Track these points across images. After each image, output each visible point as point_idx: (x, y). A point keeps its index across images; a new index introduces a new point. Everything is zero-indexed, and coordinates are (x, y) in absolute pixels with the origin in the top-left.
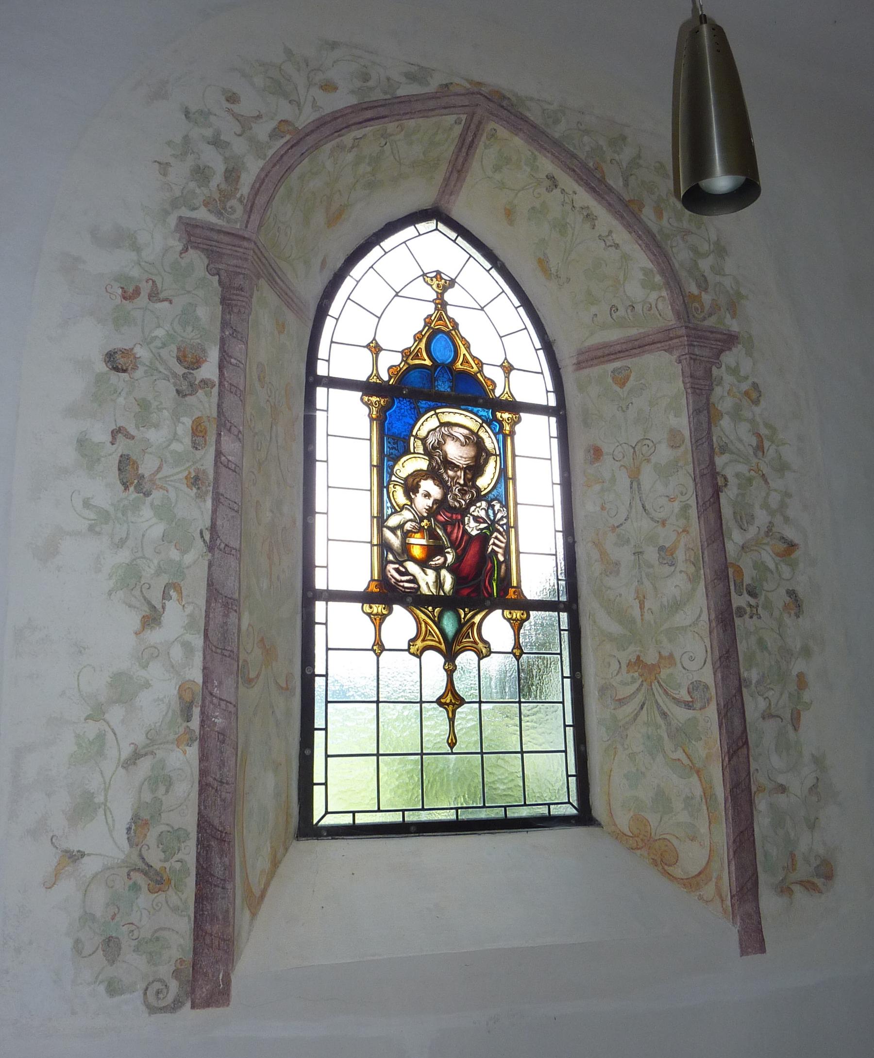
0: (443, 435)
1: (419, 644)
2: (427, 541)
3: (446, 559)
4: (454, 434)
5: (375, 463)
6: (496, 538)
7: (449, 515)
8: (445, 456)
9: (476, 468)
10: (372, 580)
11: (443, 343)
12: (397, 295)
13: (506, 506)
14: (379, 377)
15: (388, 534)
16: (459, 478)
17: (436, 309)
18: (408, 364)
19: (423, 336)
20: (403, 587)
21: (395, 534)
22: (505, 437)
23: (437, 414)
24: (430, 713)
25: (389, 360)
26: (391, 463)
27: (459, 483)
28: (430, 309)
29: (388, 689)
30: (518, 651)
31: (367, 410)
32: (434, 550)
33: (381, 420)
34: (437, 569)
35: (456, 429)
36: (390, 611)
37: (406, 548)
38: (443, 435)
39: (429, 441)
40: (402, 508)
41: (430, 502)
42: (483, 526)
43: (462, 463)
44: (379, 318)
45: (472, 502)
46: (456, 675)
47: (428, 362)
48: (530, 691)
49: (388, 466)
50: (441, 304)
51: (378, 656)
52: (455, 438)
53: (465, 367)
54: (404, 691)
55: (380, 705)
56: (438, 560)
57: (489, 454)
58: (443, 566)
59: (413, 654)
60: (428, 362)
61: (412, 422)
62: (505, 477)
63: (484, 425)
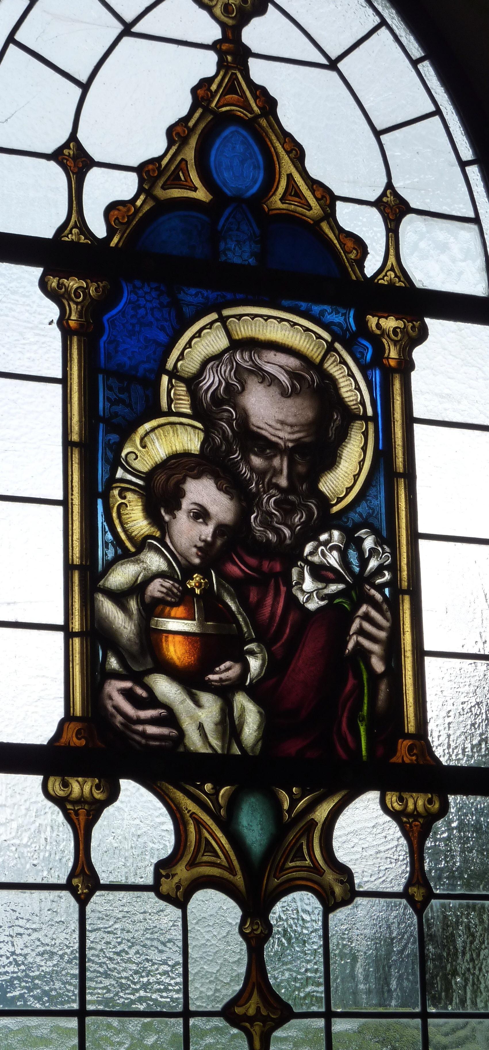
0: (239, 371)
1: (182, 872)
2: (201, 624)
3: (246, 668)
4: (268, 368)
5: (75, 437)
6: (367, 617)
7: (253, 561)
8: (244, 417)
9: (319, 451)
10: (68, 718)
11: (240, 148)
12: (128, 30)
13: (388, 539)
15: (108, 607)
16: (277, 472)
17: (221, 65)
18: (155, 198)
19: (192, 131)
20: (143, 734)
21: (124, 608)
22: (388, 374)
23: (223, 320)
24: (209, 1040)
25: (107, 189)
26: (114, 438)
27: (277, 487)
28: (207, 64)
29: (107, 982)
30: (418, 889)
31: (53, 311)
32: (216, 645)
33: (84, 334)
34: (225, 692)
35: (271, 355)
36: (113, 795)
37: (150, 638)
38: (239, 371)
39: (205, 385)
40: (142, 544)
41: (207, 531)
42: (333, 588)
43: (284, 436)
44: (85, 87)
45: (310, 532)
46: (271, 948)
47: (202, 194)
48: (448, 988)
49: (108, 445)
50: (233, 53)
51: (83, 902)
52: (269, 380)
53: (293, 207)
54: (145, 987)
55: (89, 1020)
56: (228, 671)
58: (238, 684)
60: (202, 194)
61: (163, 338)
62: (393, 472)
63: (337, 345)
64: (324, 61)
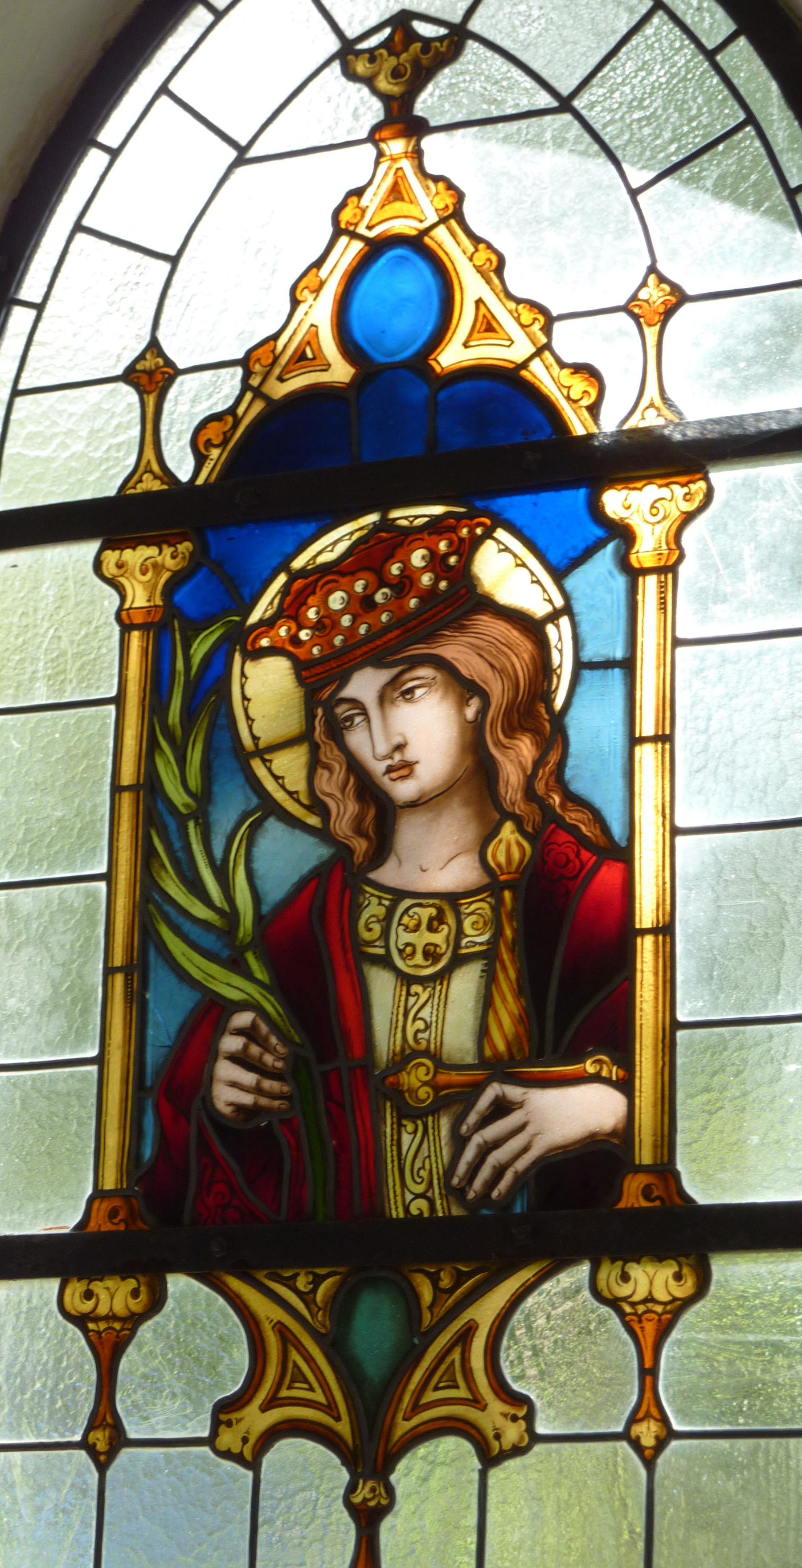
1: (255, 1419)
10: (98, 1194)
12: (242, 157)
14: (167, 475)
18: (266, 398)
25: (191, 402)
36: (156, 1303)
57: (294, 576)
59: (227, 1455)
64: (544, 100)
